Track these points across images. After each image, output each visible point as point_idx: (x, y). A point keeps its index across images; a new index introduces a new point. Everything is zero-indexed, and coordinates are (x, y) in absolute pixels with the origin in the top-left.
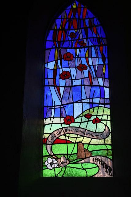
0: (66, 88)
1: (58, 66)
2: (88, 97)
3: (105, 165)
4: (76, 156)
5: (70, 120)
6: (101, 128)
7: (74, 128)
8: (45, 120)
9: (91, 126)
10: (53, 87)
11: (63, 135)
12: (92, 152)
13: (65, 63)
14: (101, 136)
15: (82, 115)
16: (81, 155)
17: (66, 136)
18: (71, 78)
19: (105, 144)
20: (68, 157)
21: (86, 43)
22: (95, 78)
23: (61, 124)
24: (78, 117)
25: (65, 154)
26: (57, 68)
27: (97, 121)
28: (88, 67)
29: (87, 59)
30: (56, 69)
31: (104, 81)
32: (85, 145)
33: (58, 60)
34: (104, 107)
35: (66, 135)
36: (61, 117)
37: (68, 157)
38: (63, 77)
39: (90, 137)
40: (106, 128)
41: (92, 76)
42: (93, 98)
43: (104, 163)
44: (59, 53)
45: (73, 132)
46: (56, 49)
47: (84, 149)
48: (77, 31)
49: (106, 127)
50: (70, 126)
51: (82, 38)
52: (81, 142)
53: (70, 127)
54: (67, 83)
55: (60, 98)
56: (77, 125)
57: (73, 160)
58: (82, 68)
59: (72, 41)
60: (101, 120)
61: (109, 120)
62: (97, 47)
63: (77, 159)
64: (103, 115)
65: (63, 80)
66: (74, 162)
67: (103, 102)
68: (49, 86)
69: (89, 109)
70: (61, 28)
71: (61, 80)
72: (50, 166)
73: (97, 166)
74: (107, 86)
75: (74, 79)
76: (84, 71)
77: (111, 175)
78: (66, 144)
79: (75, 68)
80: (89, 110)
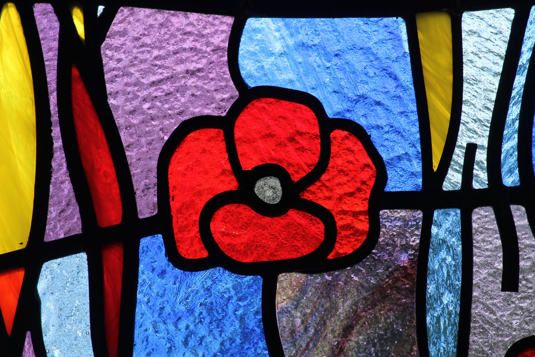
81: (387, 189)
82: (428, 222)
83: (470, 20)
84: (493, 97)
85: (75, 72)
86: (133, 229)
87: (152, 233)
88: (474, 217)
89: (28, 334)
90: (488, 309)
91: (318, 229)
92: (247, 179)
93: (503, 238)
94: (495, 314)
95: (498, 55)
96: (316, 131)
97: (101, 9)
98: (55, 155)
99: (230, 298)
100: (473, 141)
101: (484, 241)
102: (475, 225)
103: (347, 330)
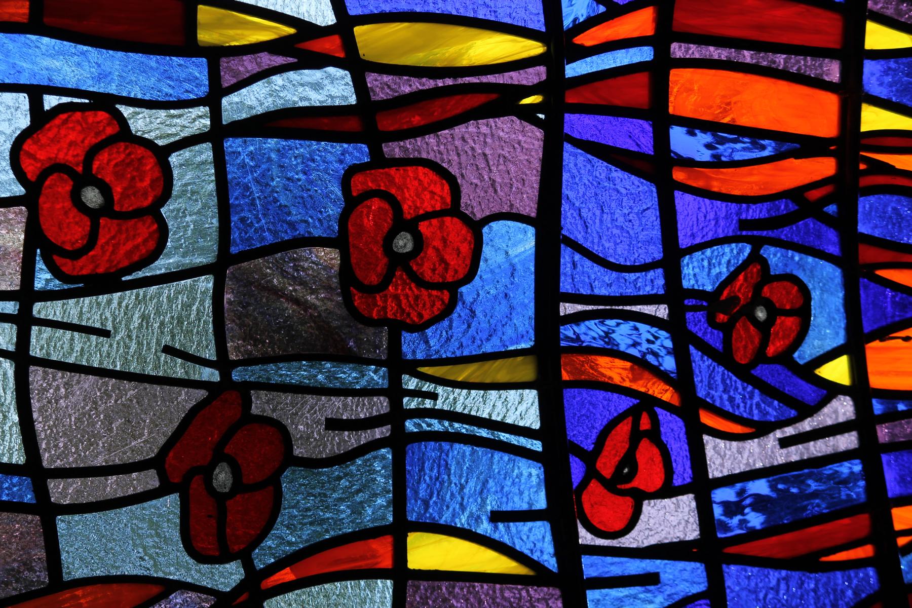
1: (248, 65)
18: (43, 278)
21: (628, 541)
26: (216, 55)
30: (205, 36)
33: (359, 68)
38: (73, 156)
44: (485, 95)
46: (535, 48)
48: (833, 390)
51: (714, 472)
59: (662, 311)
70: (873, 119)
76: (170, 503)
81: (543, 29)
82: (379, 363)
83: (531, 395)
84: (473, 413)
85: (494, 96)
86: (374, 139)
87: (371, 153)
88: (382, 398)
89: (296, 60)
90: (312, 408)
91: (374, 279)
92: (411, 226)
93: (365, 419)
94: (308, 412)
95: (505, 416)
96: (449, 279)
97: (542, 116)
98: (431, 81)
99: (321, 212)
100: (440, 398)
101: (364, 405)
102: (375, 399)
103: (296, 301)
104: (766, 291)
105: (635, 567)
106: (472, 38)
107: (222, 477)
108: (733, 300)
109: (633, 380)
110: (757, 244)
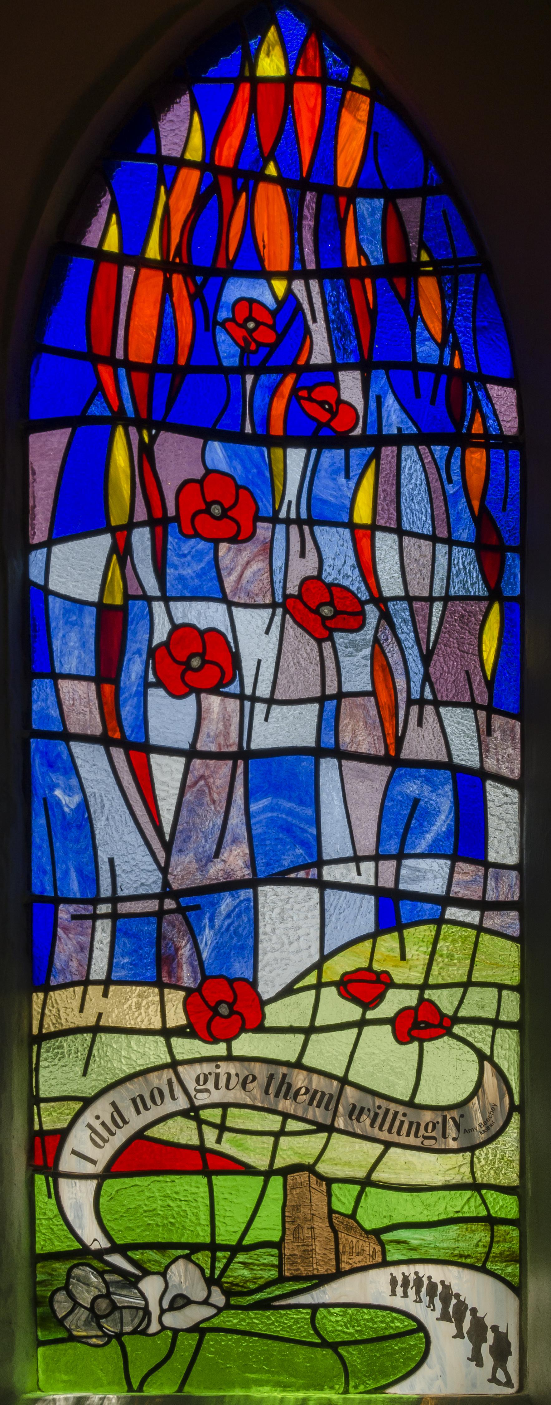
0: (197, 762)
2: (367, 844)
3: (468, 1317)
4: (276, 1262)
5: (232, 1012)
6: (448, 1072)
7: (257, 1069)
8: (38, 998)
9: (383, 1062)
10: (101, 749)
11: (184, 1113)
12: (385, 1237)
13: (187, 555)
14: (452, 1131)
15: (320, 976)
16: (307, 1254)
17: (200, 1122)
18: (234, 688)
19: (476, 1187)
20: (219, 1265)
21: (360, 407)
22: (422, 702)
23: (167, 1033)
24: (289, 991)
25: (195, 1248)
26: (127, 597)
27: (428, 1026)
28: (372, 613)
29: (362, 538)
31: (483, 727)
32: (335, 1187)
34: (480, 929)
35: (204, 1114)
36: (160, 985)
37: (219, 1265)
39: (376, 1133)
40: (490, 1079)
41: (401, 682)
42: (400, 856)
43: (461, 1307)
45: (255, 1094)
47: (331, 1211)
48: (289, 293)
49: (487, 1065)
50: (229, 1049)
52: (310, 1169)
53: (230, 1057)
54: (211, 726)
55: (156, 845)
56: (284, 1048)
57: (253, 1286)
58: (320, 611)
60: (456, 1020)
61: (508, 1025)
62: (439, 450)
63: (281, 1279)
64: (467, 984)
65: (177, 694)
66: (258, 1296)
67: (474, 894)
68: (67, 736)
69: (373, 936)
71: (157, 697)
72: (87, 1323)
73: (414, 1325)
74: (505, 772)
75: (262, 700)
76: (338, 636)
77: (503, 1379)
78: (202, 1180)
79: (274, 605)
80: (368, 944)
83: (289, 451)
104: (241, 322)
105: (373, 406)
106: (116, 464)
107: (327, 611)
108: (244, 338)
109: (283, 397)
110: (216, 323)
